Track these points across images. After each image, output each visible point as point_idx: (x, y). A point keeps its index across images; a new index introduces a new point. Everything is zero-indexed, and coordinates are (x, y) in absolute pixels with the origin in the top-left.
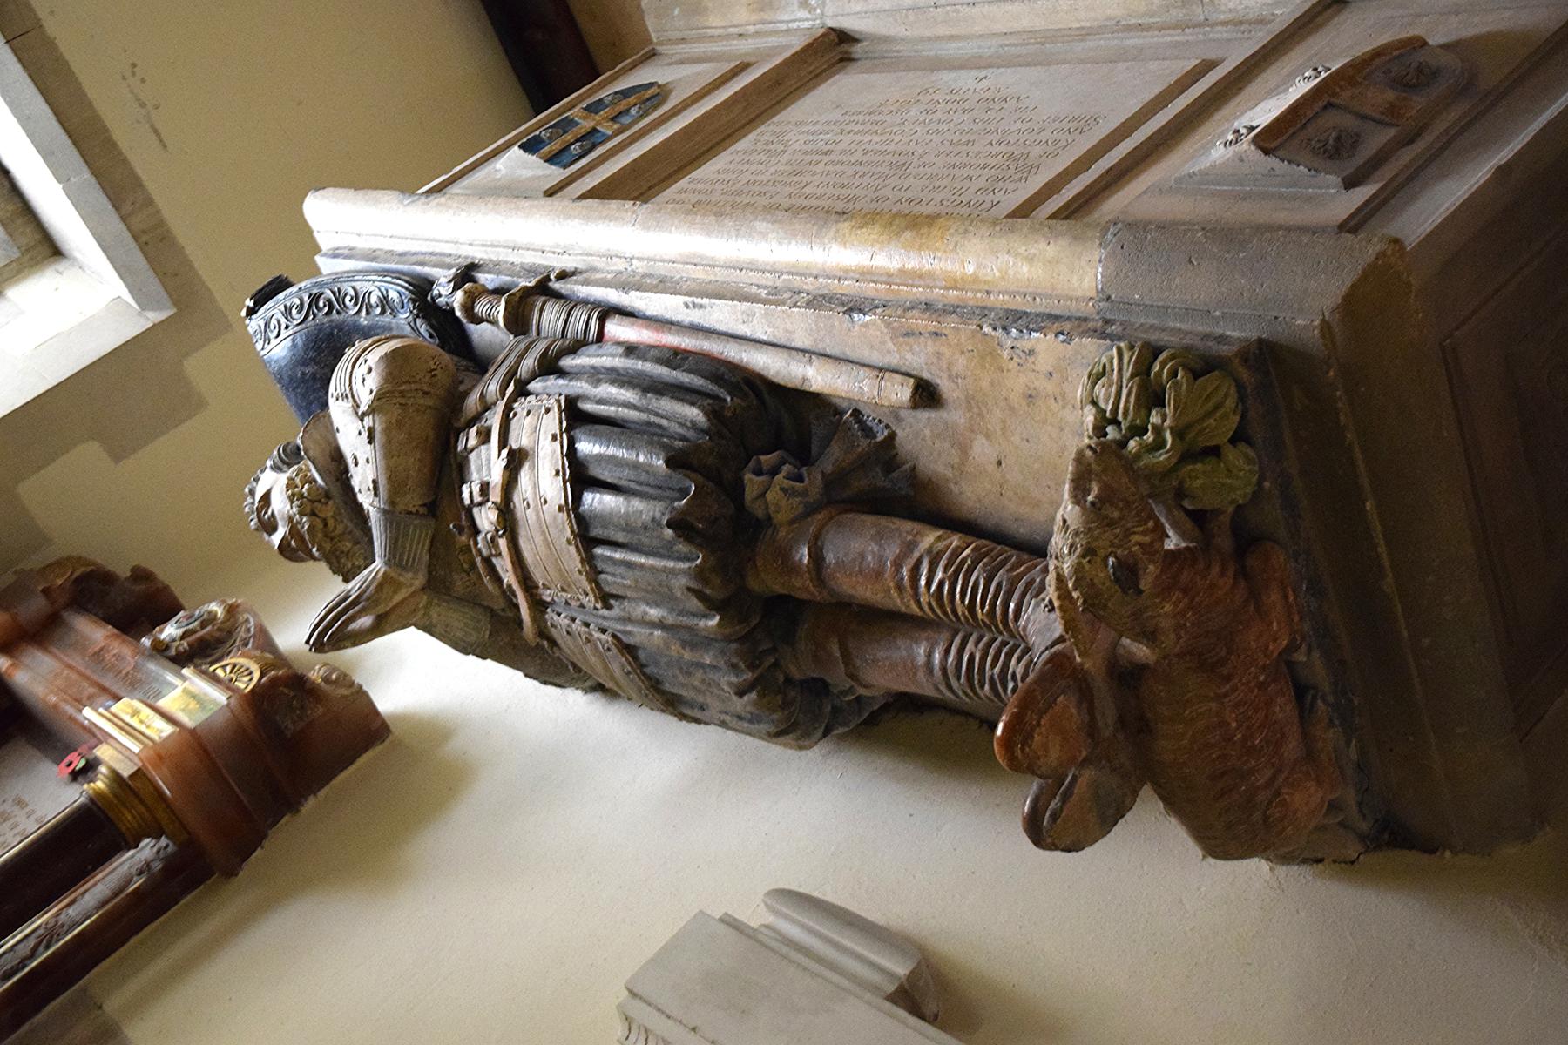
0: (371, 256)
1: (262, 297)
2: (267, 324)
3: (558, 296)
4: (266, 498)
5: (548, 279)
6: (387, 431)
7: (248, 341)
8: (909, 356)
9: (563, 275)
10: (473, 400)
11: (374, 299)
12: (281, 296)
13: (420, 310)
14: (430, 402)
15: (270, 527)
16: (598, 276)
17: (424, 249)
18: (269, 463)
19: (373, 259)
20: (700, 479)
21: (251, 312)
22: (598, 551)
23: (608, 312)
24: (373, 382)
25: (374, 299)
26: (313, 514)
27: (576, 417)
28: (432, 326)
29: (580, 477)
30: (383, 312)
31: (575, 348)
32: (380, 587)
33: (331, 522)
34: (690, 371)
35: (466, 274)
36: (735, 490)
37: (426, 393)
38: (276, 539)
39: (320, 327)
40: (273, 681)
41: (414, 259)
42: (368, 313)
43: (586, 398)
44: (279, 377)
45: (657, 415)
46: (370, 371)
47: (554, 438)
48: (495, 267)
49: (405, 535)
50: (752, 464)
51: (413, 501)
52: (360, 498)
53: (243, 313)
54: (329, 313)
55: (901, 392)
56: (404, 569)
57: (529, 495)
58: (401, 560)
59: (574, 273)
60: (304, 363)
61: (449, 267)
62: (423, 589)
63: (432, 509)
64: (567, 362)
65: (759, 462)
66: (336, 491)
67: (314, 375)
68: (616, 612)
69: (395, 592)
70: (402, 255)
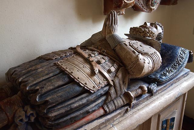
0: (179, 79)
1: (191, 57)
2: (184, 53)
3: (124, 106)
4: (156, 28)
5: (130, 107)
6: (132, 55)
7: (186, 48)
8: (122, 125)
9: (127, 111)
10: (120, 75)
11: (167, 73)
12: (187, 60)
13: (156, 79)
14: (129, 67)
15: (152, 24)
16: (119, 116)
17: (168, 89)
18: (162, 33)
19: (177, 79)
20: (38, 104)
21: (190, 52)
22: (58, 71)
23: (106, 114)
24: (142, 61)
25: (167, 73)
26: (143, 32)
27: (87, 91)
28: (152, 78)
29: (72, 81)
30: (164, 73)
31: (105, 102)
32: (110, 30)
33: (140, 33)
34: (67, 120)
35: (151, 92)
36: (33, 107)
37: (131, 68)
38: (148, 24)
39: (173, 61)
40: (122, 3)
41: (168, 86)
42: (167, 70)
43: (87, 96)
44: (175, 47)
45: (63, 107)
46: (144, 63)
47: (86, 84)
48: (147, 99)
49: (114, 42)
50: (35, 114)
51: (117, 49)
52: (140, 43)
53: (191, 51)
54: (174, 64)
55: (55, 109)
56: (109, 37)
57: (85, 69)
58: (111, 38)
59: (124, 114)
60: (173, 52)
61: (156, 92)
62: (105, 37)
63: (114, 50)
64: (103, 98)
65: (33, 116)
66: (144, 39)
67: (168, 52)
68: (53, 63)
69: (107, 32)
70: (172, 84)
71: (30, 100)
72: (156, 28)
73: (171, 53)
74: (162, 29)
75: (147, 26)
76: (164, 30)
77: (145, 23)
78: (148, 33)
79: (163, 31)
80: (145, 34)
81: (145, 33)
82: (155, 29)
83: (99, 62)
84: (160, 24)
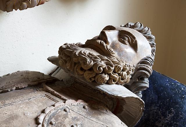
4: (134, 46)
26: (91, 69)
33: (81, 73)
38: (112, 36)
67: (165, 116)
71: (125, 104)
72: (134, 46)
73: (173, 118)
74: (152, 45)
75: (106, 42)
76: (159, 49)
77: (103, 36)
78: (105, 72)
79: (153, 51)
80: (97, 74)
81: (95, 74)
82: (129, 50)
83: (88, 62)
84: (146, 29)
